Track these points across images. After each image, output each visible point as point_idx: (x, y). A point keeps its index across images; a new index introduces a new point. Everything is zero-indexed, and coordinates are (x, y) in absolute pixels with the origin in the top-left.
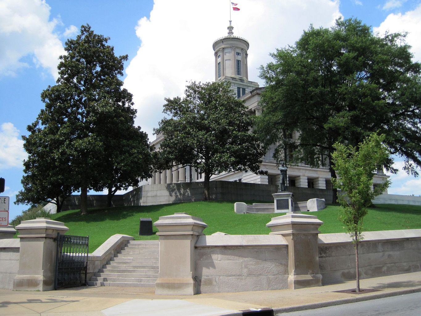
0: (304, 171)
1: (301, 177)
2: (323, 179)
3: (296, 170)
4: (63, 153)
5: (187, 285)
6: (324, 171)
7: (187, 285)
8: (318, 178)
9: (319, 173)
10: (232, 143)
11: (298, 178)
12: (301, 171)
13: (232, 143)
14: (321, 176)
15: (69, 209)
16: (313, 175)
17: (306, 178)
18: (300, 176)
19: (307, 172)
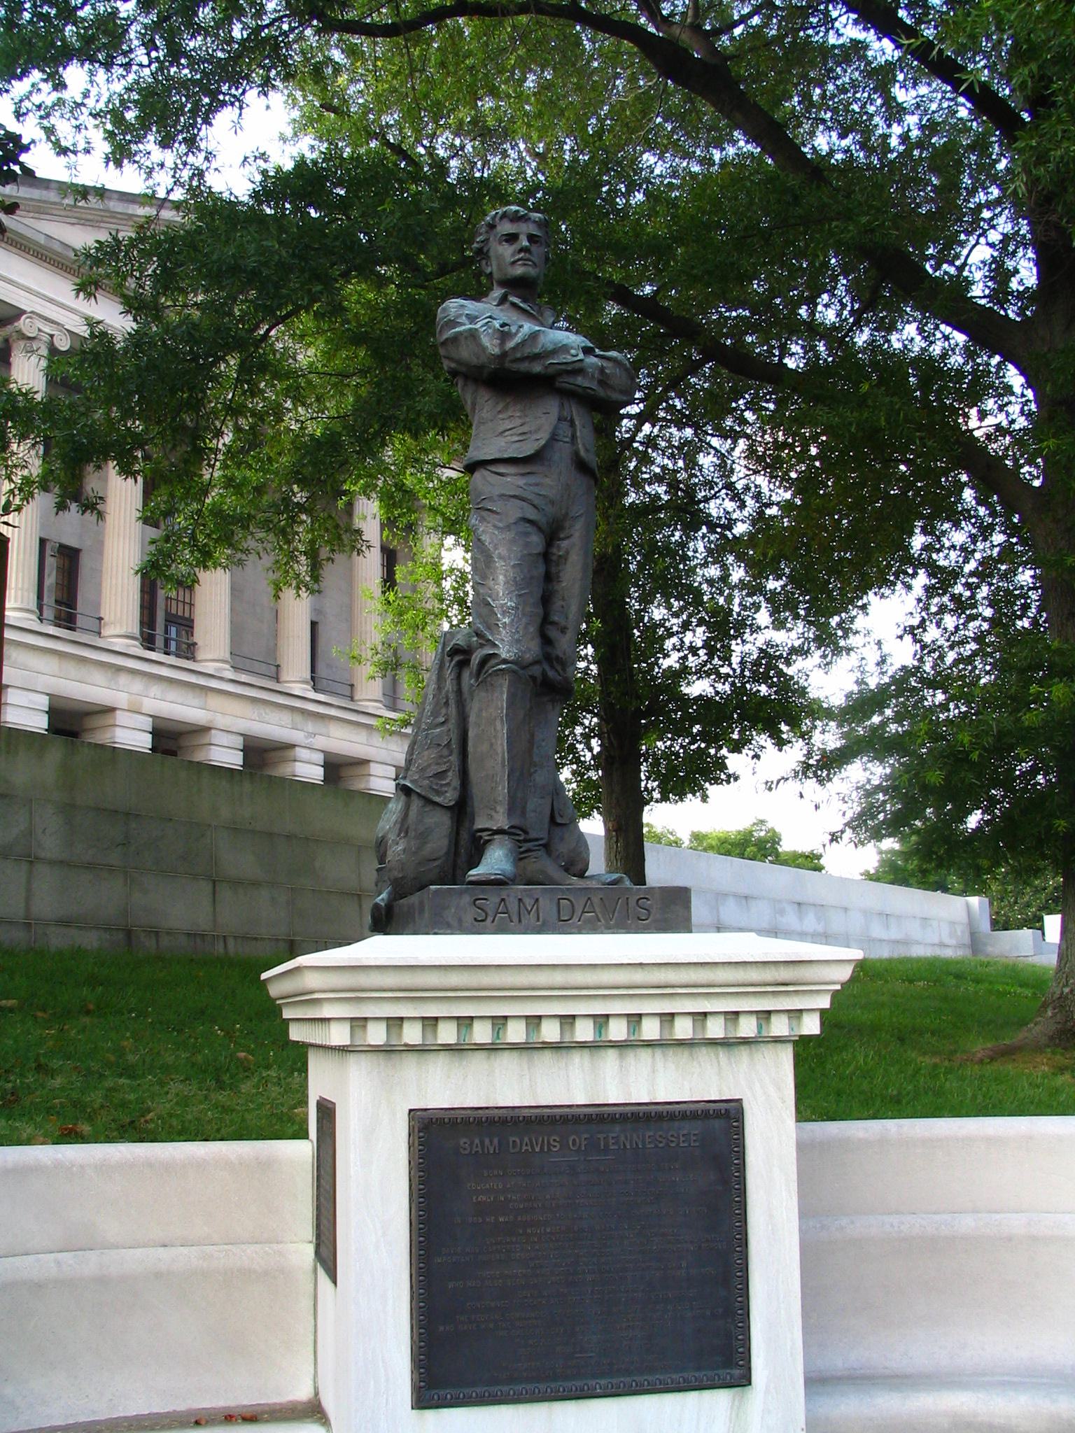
0: (137, 685)
1: (121, 718)
2: (233, 737)
3: (98, 676)
4: (779, 625)
5: (600, 1036)
6: (254, 700)
7: (600, 1036)
8: (205, 730)
9: (215, 701)
10: (641, 419)
11: (361, 770)
12: (123, 679)
13: (641, 419)
14: (221, 721)
15: (307, 1114)
16: (273, 727)
17: (147, 723)
18: (368, 761)
19: (155, 690)
